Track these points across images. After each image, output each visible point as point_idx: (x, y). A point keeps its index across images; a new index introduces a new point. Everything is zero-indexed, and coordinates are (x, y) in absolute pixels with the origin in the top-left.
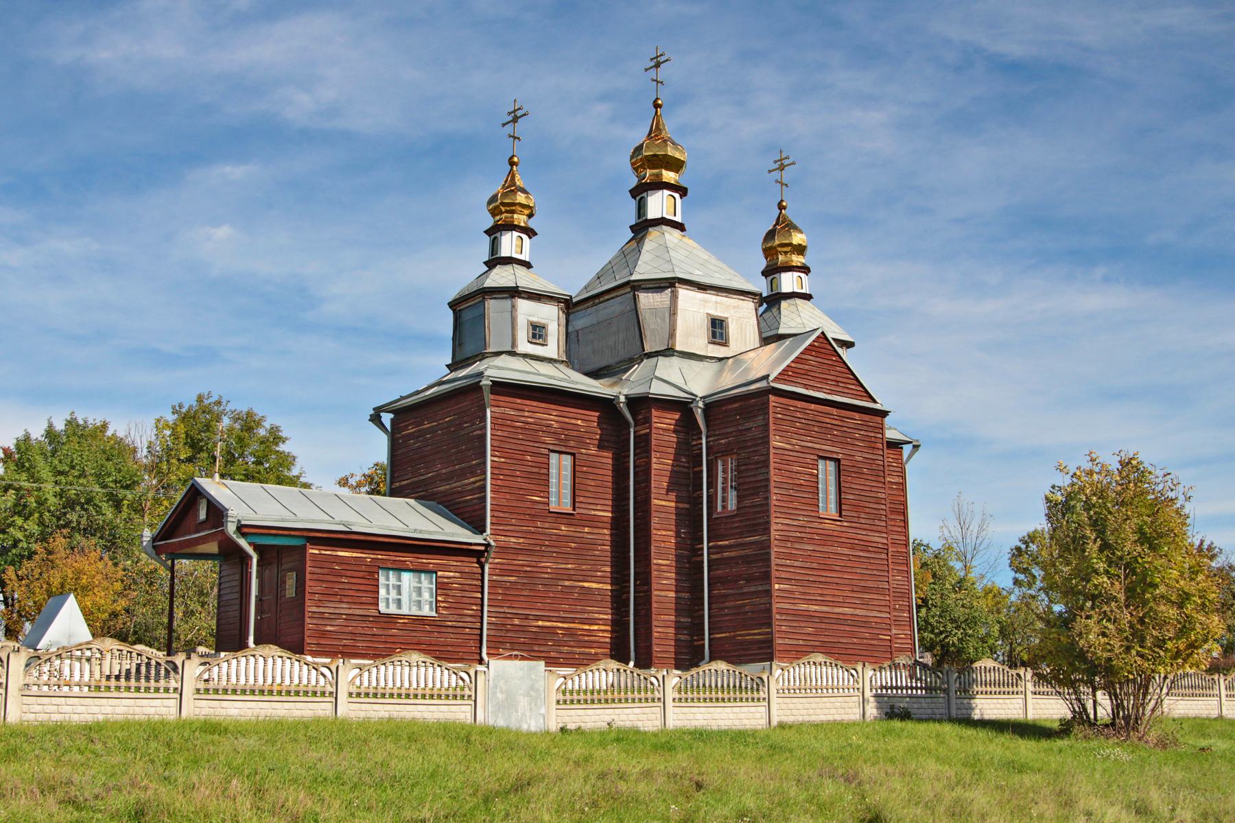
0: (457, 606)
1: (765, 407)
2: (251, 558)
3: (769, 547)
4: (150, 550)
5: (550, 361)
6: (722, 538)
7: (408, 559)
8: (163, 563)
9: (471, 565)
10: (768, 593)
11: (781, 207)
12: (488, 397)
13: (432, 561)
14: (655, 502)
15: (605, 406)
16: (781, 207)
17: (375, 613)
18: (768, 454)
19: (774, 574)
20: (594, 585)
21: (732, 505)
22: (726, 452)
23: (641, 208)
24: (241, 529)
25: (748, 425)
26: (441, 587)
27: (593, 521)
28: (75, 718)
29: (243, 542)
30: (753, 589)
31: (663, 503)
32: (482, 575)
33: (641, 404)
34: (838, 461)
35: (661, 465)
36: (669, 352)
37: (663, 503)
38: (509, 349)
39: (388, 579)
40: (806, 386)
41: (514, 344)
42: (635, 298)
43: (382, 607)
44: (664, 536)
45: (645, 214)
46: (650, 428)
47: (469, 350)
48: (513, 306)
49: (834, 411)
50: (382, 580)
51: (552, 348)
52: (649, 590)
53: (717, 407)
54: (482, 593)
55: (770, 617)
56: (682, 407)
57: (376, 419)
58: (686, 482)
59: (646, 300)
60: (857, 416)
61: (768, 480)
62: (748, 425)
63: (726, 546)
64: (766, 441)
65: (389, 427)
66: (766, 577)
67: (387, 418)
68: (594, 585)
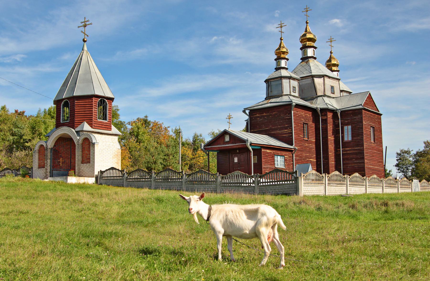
0: (288, 165)
1: (361, 113)
2: (251, 152)
3: (364, 150)
4: (204, 150)
5: (297, 97)
6: (347, 148)
7: (279, 152)
8: (206, 153)
9: (290, 154)
10: (364, 163)
11: (331, 53)
12: (293, 108)
13: (284, 153)
14: (329, 137)
15: (313, 111)
16: (331, 53)
17: (274, 167)
18: (362, 126)
19: (365, 158)
20: (312, 160)
21: (350, 139)
22: (347, 124)
23: (305, 53)
24: (251, 144)
25: (355, 117)
26: (285, 160)
27: (311, 142)
28: (311, 194)
29: (250, 148)
30: (358, 161)
31: (331, 138)
32: (293, 157)
33: (325, 111)
34: (373, 128)
35: (330, 127)
36: (325, 95)
37: (331, 138)
38: (289, 93)
39: (277, 158)
40: (367, 107)
41: (290, 93)
42: (313, 80)
43: (276, 166)
44: (331, 147)
45: (307, 54)
46: (327, 117)
47: (275, 93)
48: (290, 82)
49: (373, 114)
50: (276, 159)
51: (297, 94)
52: (328, 161)
53: (345, 113)
54: (293, 162)
55: (364, 169)
56: (334, 112)
57: (244, 112)
58: (336, 132)
59: (316, 80)
60: (376, 115)
61: (363, 133)
62: (355, 117)
63: (348, 150)
64: (362, 122)
65: (248, 114)
66: (363, 158)
67: (247, 112)
68: (312, 160)
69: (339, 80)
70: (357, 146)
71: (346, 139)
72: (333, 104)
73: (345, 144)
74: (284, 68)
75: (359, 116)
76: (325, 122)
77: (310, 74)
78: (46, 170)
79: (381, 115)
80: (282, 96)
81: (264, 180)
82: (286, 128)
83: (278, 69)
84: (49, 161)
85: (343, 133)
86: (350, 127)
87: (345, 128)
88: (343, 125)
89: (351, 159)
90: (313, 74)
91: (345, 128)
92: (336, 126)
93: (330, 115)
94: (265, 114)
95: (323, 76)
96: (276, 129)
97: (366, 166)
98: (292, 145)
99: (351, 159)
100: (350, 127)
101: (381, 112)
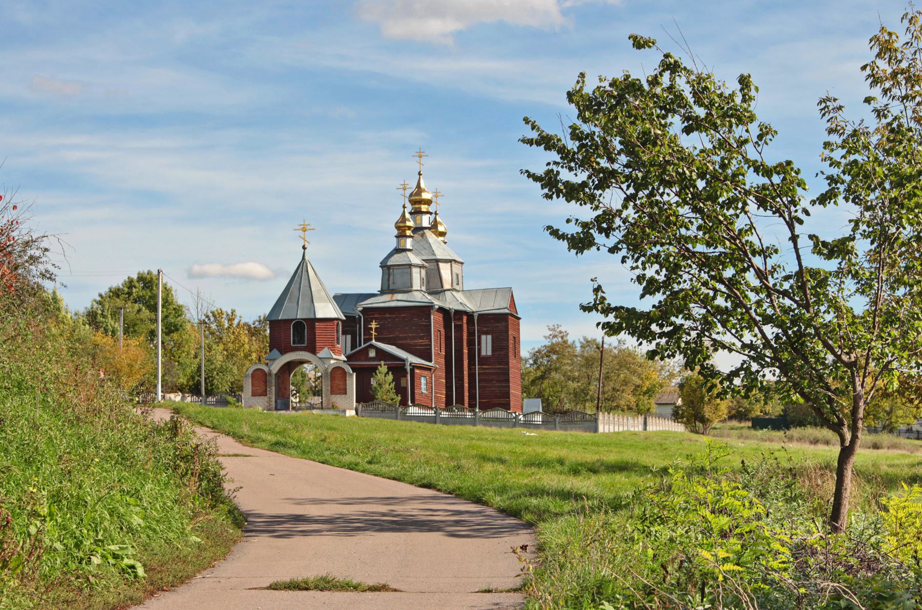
21: (490, 353)
22: (486, 333)
33: (459, 314)
53: (485, 318)
56: (470, 315)
58: (471, 343)
59: (441, 265)
69: (462, 263)
70: (500, 364)
71: (483, 353)
72: (471, 306)
73: (484, 360)
74: (410, 250)
75: (504, 323)
76: (459, 328)
77: (433, 257)
78: (270, 398)
79: (519, 319)
80: (410, 291)
81: (612, 427)
82: (422, 338)
83: (398, 251)
84: (274, 388)
85: (479, 344)
86: (489, 337)
87: (483, 337)
88: (481, 333)
89: (491, 381)
90: (439, 257)
91: (483, 337)
92: (471, 334)
93: (465, 318)
94: (388, 315)
95: (450, 261)
96: (405, 338)
97: (512, 391)
98: (431, 361)
99: (491, 381)
100: (489, 337)
101: (519, 316)
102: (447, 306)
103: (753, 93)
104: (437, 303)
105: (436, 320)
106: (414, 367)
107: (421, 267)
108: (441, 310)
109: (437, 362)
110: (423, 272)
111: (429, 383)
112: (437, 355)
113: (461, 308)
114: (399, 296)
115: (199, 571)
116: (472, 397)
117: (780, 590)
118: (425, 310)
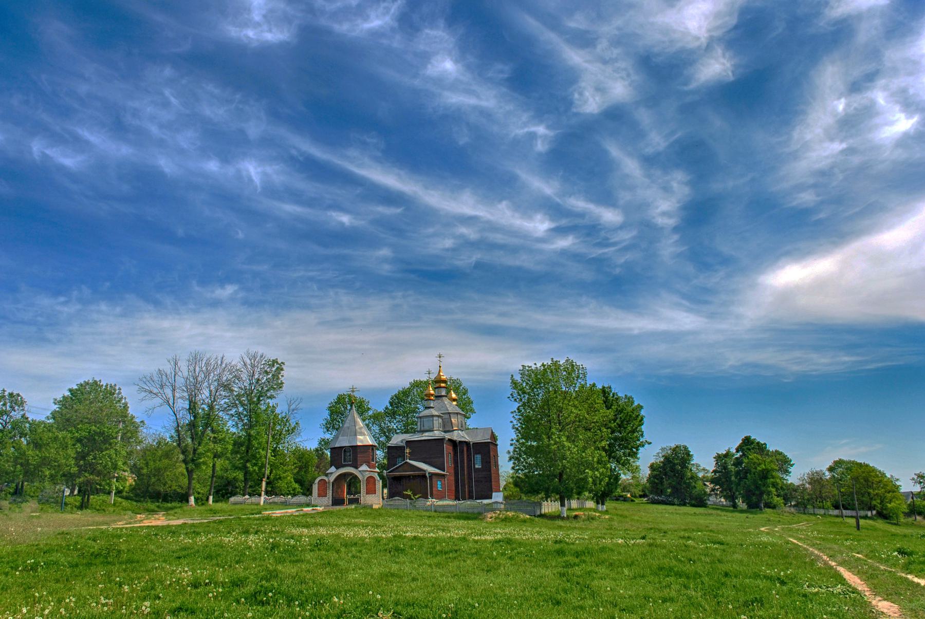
56: (467, 443)
58: (469, 460)
73: (477, 470)
76: (462, 452)
102: (455, 438)
103: (143, 394)
104: (448, 436)
105: (447, 449)
106: (432, 475)
107: (438, 416)
108: (451, 441)
109: (448, 471)
110: (440, 420)
111: (443, 485)
112: (448, 467)
113: (463, 440)
114: (427, 434)
115: (93, 451)
116: (470, 492)
117: (394, 515)
118: (441, 440)
